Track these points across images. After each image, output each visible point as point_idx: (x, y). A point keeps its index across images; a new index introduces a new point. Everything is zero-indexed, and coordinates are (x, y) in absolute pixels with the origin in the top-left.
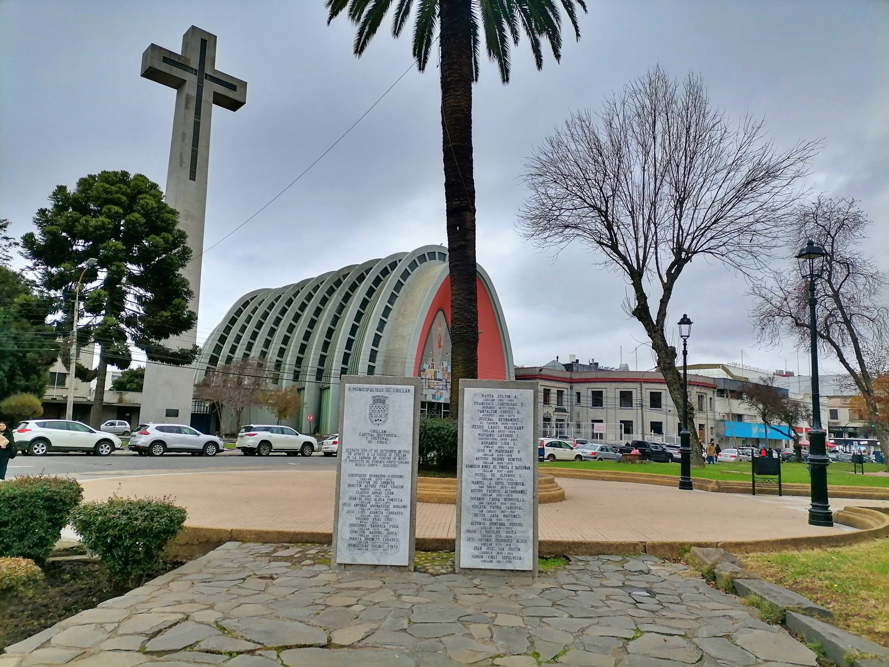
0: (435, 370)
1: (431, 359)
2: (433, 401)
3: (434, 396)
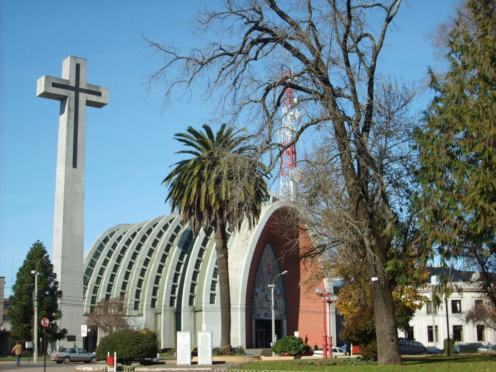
2: (266, 318)
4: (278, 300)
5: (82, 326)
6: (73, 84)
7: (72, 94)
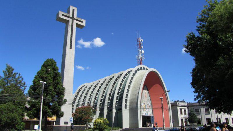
2: (146, 115)
3: (145, 113)
6: (71, 16)
7: (70, 20)
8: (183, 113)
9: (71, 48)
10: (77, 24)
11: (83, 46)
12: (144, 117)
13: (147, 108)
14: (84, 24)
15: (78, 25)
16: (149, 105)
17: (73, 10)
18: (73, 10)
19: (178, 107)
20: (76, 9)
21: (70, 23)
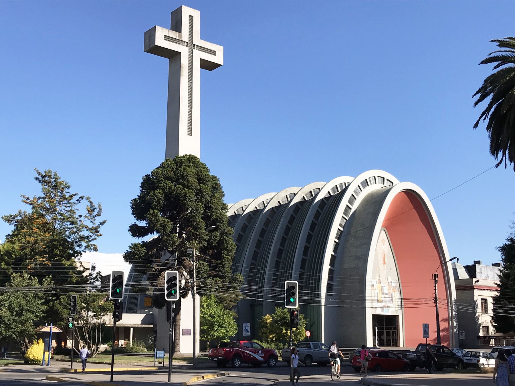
0: (382, 285)
1: (378, 275)
4: (393, 293)
5: (244, 325)
8: (490, 301)
9: (190, 133)
10: (202, 60)
11: (52, 294)
12: (377, 319)
13: (387, 294)
14: (218, 59)
15: (206, 65)
16: (394, 285)
17: (191, 18)
18: (191, 18)
19: (476, 292)
20: (196, 14)
21: (184, 61)
